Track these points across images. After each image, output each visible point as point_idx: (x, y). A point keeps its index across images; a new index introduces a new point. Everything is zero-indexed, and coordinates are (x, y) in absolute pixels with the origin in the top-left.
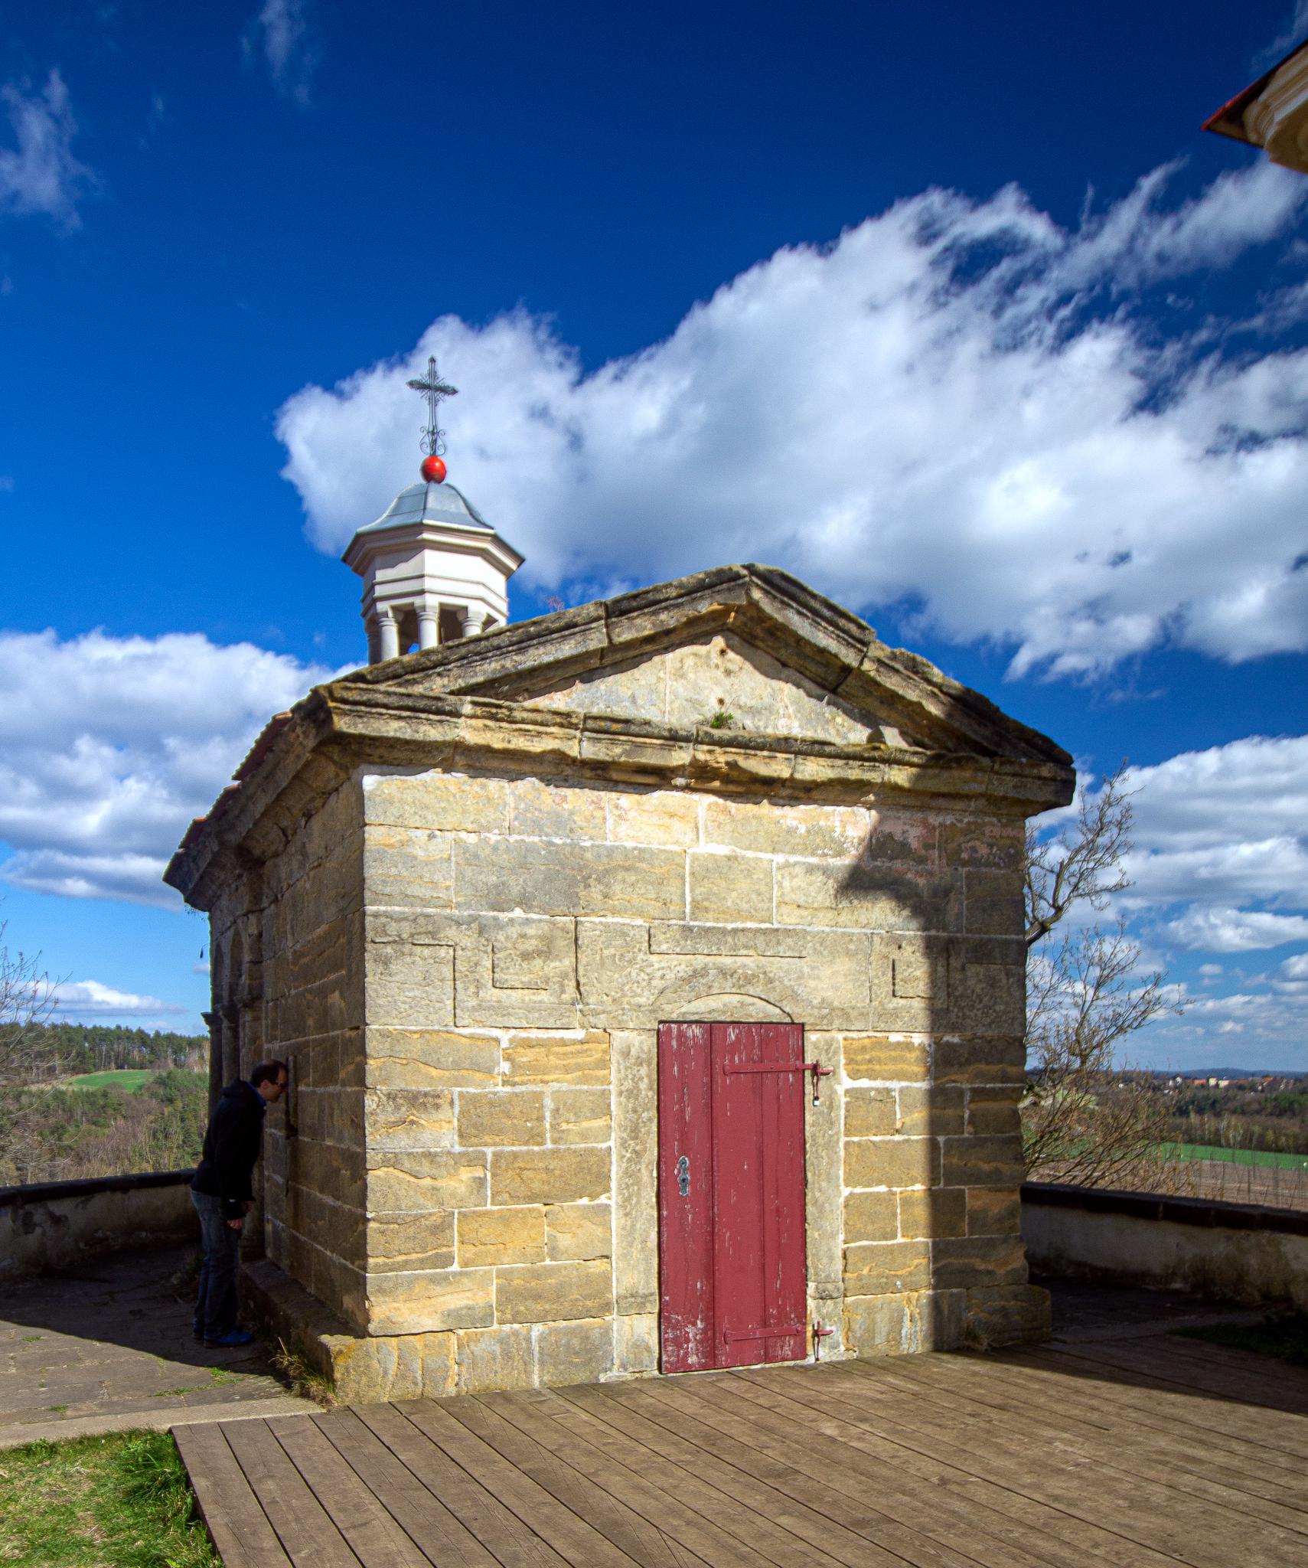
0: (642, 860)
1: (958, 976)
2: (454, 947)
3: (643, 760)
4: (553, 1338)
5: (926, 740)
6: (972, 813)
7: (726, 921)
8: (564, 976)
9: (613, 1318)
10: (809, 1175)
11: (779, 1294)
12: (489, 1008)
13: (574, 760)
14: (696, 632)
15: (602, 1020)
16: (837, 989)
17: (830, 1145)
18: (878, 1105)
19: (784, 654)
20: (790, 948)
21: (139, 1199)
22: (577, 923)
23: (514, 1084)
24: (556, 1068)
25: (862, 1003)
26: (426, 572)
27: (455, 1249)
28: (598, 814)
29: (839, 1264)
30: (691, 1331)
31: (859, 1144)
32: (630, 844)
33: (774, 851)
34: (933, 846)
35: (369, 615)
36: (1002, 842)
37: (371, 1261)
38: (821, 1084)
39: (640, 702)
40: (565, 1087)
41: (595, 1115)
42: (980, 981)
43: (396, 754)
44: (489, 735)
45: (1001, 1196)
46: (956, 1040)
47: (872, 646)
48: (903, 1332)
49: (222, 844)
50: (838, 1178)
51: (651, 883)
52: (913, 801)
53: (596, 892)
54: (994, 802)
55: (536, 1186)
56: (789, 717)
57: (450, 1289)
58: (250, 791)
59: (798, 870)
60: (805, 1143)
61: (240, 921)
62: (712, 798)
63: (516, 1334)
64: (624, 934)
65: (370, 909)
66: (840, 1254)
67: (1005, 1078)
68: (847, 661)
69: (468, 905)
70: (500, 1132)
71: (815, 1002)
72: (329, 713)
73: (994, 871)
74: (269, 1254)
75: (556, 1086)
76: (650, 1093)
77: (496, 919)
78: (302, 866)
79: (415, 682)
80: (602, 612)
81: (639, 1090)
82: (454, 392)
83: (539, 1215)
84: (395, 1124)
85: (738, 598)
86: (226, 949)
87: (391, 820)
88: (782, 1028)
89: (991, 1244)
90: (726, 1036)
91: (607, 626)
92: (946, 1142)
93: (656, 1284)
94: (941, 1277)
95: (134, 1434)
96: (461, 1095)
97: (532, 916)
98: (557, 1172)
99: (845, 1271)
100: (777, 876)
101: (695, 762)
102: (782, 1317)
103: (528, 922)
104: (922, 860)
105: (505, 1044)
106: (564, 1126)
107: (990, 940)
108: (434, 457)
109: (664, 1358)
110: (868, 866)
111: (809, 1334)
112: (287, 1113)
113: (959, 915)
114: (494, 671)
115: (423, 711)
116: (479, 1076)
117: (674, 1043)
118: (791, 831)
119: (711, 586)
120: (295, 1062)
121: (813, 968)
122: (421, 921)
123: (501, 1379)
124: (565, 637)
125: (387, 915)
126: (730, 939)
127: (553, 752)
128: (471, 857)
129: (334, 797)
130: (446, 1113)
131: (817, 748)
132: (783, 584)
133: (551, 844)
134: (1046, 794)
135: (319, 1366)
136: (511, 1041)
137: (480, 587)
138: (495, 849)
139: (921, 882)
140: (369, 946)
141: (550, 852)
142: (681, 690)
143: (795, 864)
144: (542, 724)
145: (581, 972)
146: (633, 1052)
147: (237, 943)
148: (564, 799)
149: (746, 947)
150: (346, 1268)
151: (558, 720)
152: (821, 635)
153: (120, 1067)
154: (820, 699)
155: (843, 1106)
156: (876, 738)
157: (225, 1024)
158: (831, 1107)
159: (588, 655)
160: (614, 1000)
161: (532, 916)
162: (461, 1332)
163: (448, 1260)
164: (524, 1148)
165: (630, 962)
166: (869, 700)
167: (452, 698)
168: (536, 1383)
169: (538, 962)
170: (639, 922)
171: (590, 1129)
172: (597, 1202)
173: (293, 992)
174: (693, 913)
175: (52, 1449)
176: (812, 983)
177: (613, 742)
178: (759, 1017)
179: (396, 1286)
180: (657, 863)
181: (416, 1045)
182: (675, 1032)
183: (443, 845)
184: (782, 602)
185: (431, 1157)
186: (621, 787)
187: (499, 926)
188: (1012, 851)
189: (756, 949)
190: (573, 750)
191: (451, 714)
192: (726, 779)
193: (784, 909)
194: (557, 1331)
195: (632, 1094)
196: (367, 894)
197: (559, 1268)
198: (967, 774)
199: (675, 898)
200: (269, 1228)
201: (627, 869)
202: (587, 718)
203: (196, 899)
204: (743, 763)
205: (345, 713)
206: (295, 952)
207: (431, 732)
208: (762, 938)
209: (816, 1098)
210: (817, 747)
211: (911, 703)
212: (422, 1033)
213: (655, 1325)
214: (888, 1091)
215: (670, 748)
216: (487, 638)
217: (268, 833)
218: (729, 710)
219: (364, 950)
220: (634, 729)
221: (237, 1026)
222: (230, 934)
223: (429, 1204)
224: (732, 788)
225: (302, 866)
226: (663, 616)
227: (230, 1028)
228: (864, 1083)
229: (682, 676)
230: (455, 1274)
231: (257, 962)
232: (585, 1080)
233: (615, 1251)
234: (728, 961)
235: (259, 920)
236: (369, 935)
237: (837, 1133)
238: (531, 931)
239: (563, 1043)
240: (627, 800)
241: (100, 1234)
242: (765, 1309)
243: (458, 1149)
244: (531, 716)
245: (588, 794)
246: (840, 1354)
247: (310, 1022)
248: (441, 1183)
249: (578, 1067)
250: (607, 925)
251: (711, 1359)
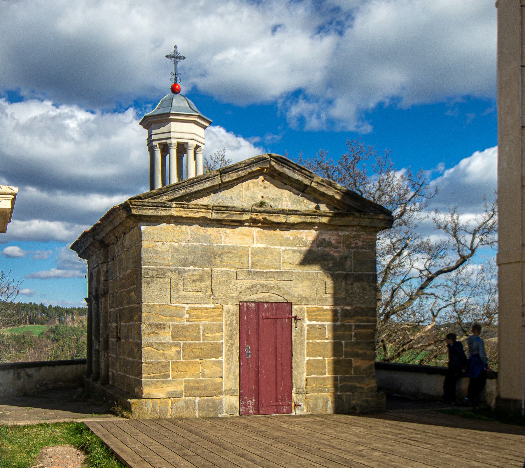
0: (234, 250)
1: (350, 287)
2: (170, 278)
3: (233, 219)
4: (203, 402)
5: (338, 207)
6: (355, 231)
7: (264, 269)
8: (207, 287)
9: (223, 397)
10: (294, 353)
11: (282, 391)
12: (181, 298)
13: (210, 219)
14: (253, 176)
15: (220, 301)
16: (304, 291)
17: (302, 343)
18: (319, 330)
19: (285, 181)
20: (287, 278)
21: (58, 369)
22: (211, 270)
23: (190, 322)
24: (204, 316)
25: (313, 295)
26: (172, 130)
27: (170, 373)
28: (218, 235)
29: (304, 383)
30: (250, 402)
31: (312, 343)
32: (230, 245)
33: (281, 245)
34: (340, 243)
35: (150, 145)
36: (367, 241)
37: (143, 375)
38: (298, 323)
39: (234, 199)
40: (207, 323)
41: (217, 332)
42: (359, 288)
43: (151, 219)
44: (181, 213)
45: (367, 362)
46: (349, 308)
47: (315, 178)
48: (328, 406)
49: (94, 239)
50: (304, 354)
51: (237, 257)
52: (332, 228)
53: (218, 260)
54: (364, 228)
55: (197, 354)
56: (287, 201)
57: (169, 385)
58: (105, 224)
59: (290, 252)
60: (292, 342)
61: (100, 265)
62: (259, 229)
63: (190, 400)
64: (228, 274)
65: (143, 267)
66: (305, 379)
67: (368, 321)
68: (306, 183)
69: (175, 265)
70: (185, 337)
71: (296, 295)
72: (130, 209)
73: (364, 250)
74: (111, 383)
75: (204, 322)
76: (236, 325)
77: (184, 269)
78: (122, 249)
79: (157, 198)
80: (218, 173)
81: (233, 324)
82: (184, 58)
83: (198, 363)
84: (151, 333)
85: (266, 165)
86: (94, 275)
87: (150, 239)
88: (284, 304)
89: (363, 378)
90: (263, 307)
91: (221, 177)
92: (345, 343)
93: (238, 386)
94: (336, 387)
95: (72, 422)
96: (172, 325)
97: (197, 268)
98: (204, 350)
99: (307, 385)
100: (282, 254)
101: (251, 218)
102: (283, 399)
103: (195, 270)
104: (336, 247)
105: (187, 309)
106: (207, 335)
107: (362, 274)
108: (175, 84)
109: (241, 410)
110: (315, 249)
111: (293, 405)
112: (117, 333)
113: (351, 265)
114: (183, 193)
115: (160, 207)
116: (178, 319)
117: (245, 309)
118: (287, 239)
119: (256, 162)
120: (120, 315)
121: (295, 284)
122: (160, 270)
123: (185, 414)
124: (206, 181)
125: (148, 269)
126: (265, 275)
127: (202, 217)
128: (176, 250)
129: (132, 230)
130: (168, 330)
131: (294, 213)
132: (282, 160)
133: (203, 245)
134: (382, 224)
135: (128, 408)
136: (189, 308)
137: (193, 135)
138: (184, 247)
139: (336, 255)
140: (143, 278)
141: (202, 248)
142: (248, 194)
143: (289, 250)
144: (198, 209)
145: (213, 286)
146: (231, 312)
147: (98, 273)
148: (207, 231)
149: (271, 277)
150: (136, 379)
151: (204, 207)
152: (296, 175)
153: (31, 323)
154: (298, 195)
155: (306, 330)
156: (317, 208)
157: (94, 302)
158: (302, 330)
159: (214, 186)
160: (224, 295)
161: (197, 268)
162: (172, 399)
163: (168, 376)
164: (193, 342)
165: (230, 283)
166: (316, 194)
167: (169, 203)
168: (197, 416)
169: (198, 283)
170: (233, 270)
171: (216, 336)
172: (218, 359)
173: (119, 291)
174: (252, 267)
175: (48, 425)
176: (295, 289)
177: (223, 213)
178: (276, 300)
179: (151, 383)
180: (239, 250)
181: (158, 309)
182: (245, 305)
183: (167, 246)
184: (282, 166)
185: (163, 344)
186: (227, 226)
187: (185, 271)
188: (371, 243)
189: (274, 278)
190: (209, 216)
191: (169, 207)
192: (263, 223)
193: (285, 265)
194: (204, 400)
195: (230, 325)
196: (142, 262)
197: (205, 380)
198: (351, 219)
199: (246, 262)
200: (110, 374)
201: (229, 253)
202: (213, 206)
203: (82, 255)
204: (268, 218)
205: (135, 209)
206: (120, 278)
207: (163, 213)
208: (276, 274)
209: (296, 327)
210: (294, 212)
211: (330, 196)
212: (160, 305)
213: (238, 400)
214: (323, 325)
215: (243, 214)
216: (180, 184)
217: (110, 237)
218: (266, 200)
219: (141, 280)
220: (229, 209)
221: (99, 303)
222: (96, 269)
223: (162, 358)
224: (265, 225)
225: (122, 249)
226: (240, 173)
227: (96, 304)
228: (314, 322)
229: (249, 189)
230: (170, 381)
231: (106, 281)
232: (214, 321)
233: (224, 375)
234: (264, 282)
235: (107, 266)
236: (143, 275)
237: (304, 339)
238: (196, 273)
239: (206, 308)
240: (228, 231)
241: (44, 382)
242: (277, 396)
243: (171, 341)
244: (195, 206)
245: (215, 229)
246: (305, 412)
247: (125, 302)
248: (166, 352)
249: (212, 316)
250: (222, 271)
251: (257, 412)
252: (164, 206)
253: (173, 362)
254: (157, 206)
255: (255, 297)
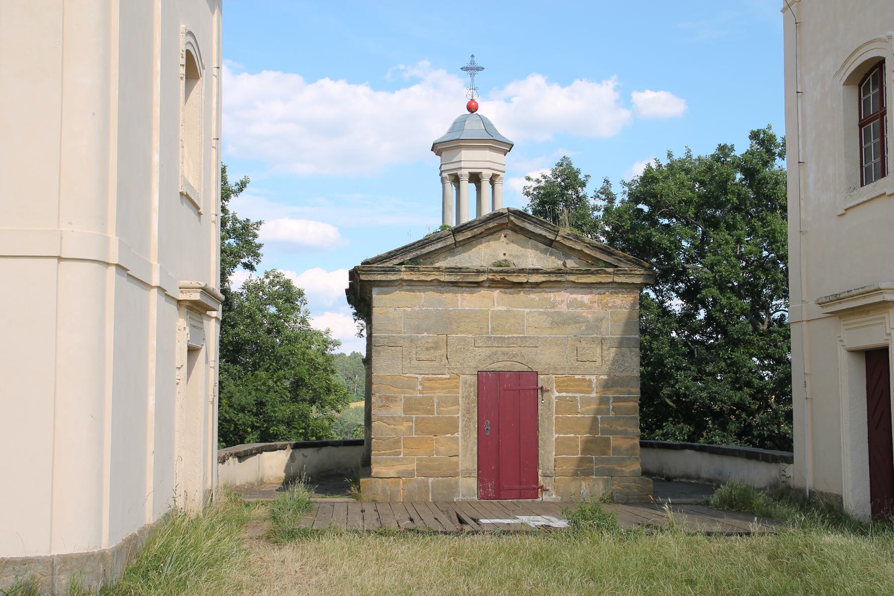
8: (442, 356)
15: (455, 371)
29: (552, 463)
33: (525, 308)
40: (442, 395)
64: (465, 340)
75: (438, 395)
104: (590, 308)
108: (472, 100)
113: (607, 328)
116: (411, 391)
131: (536, 271)
139: (590, 316)
158: (549, 403)
169: (432, 351)
176: (541, 357)
185: (394, 418)
190: (442, 278)
204: (506, 278)
228: (564, 394)
232: (449, 392)
239: (441, 379)
243: (403, 415)
249: (447, 388)
252: (391, 270)
253: (405, 438)
254: (386, 271)
255: (496, 367)
